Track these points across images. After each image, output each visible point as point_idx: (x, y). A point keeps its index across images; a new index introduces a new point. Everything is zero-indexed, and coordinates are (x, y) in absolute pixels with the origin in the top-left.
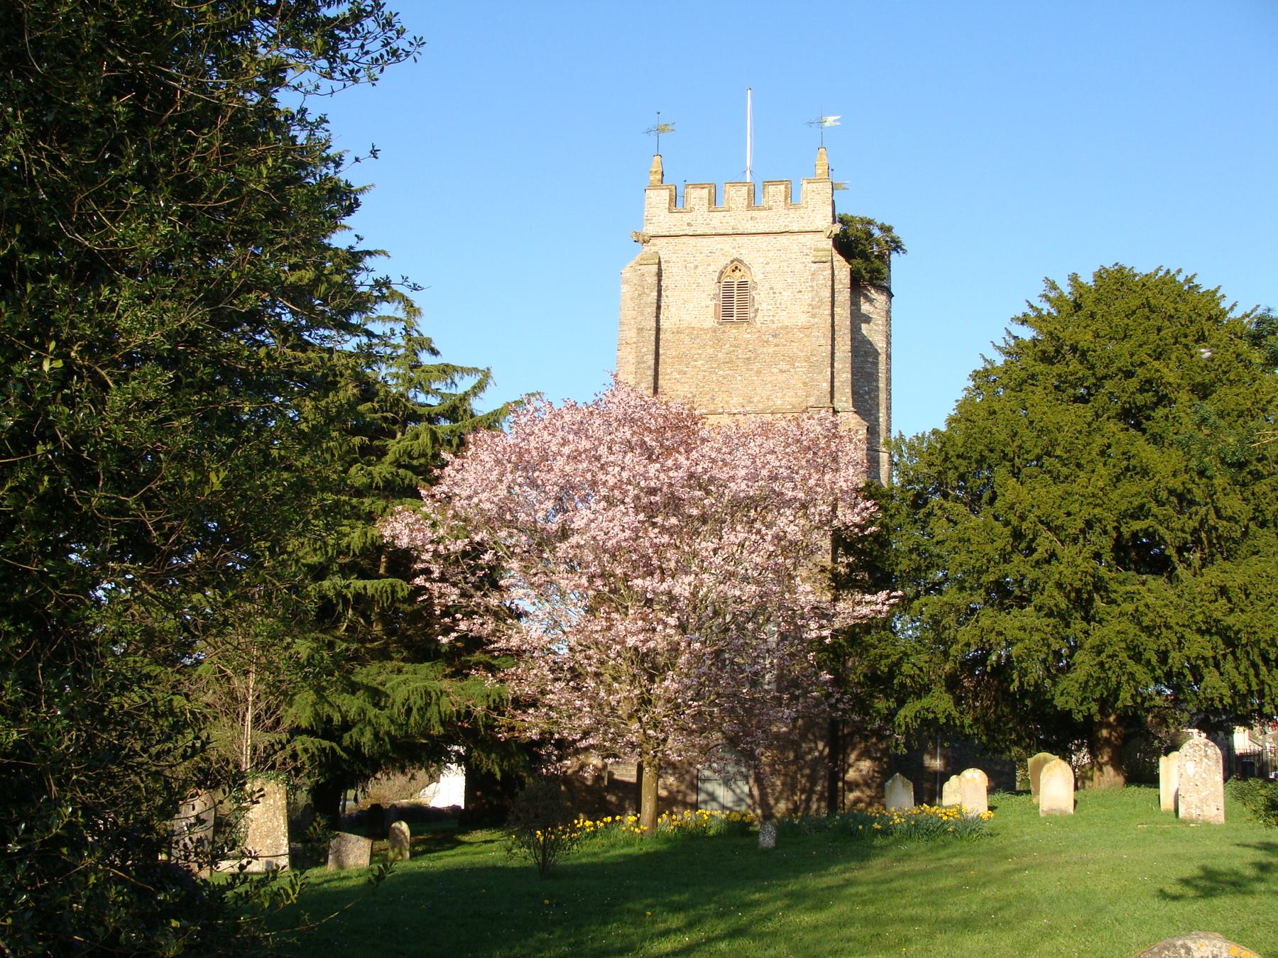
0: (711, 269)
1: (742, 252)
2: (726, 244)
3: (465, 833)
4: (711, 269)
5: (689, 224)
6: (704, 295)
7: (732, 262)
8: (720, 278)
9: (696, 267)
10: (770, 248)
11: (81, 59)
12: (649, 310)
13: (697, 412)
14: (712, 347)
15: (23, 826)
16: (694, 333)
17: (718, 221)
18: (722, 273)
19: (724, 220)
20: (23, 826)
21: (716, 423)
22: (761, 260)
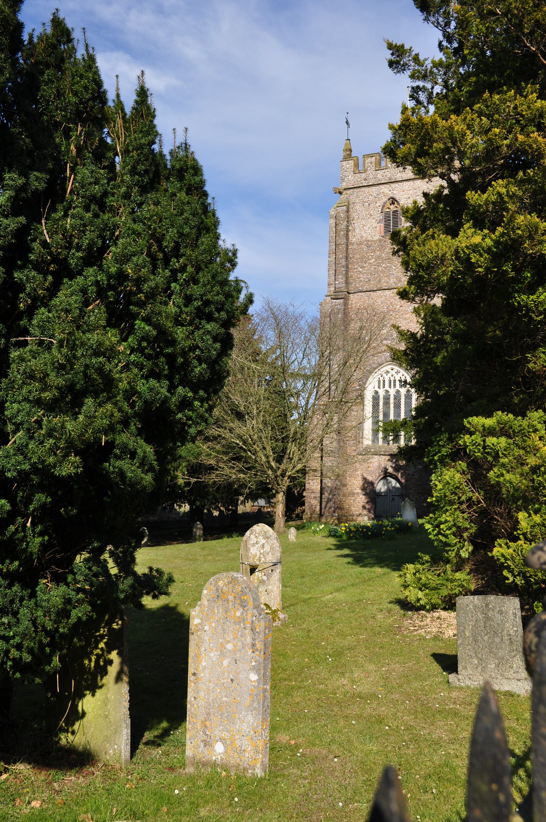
0: (378, 204)
1: (395, 192)
2: (385, 189)
3: (282, 573)
4: (378, 204)
5: (365, 179)
6: (374, 221)
7: (389, 199)
8: (382, 209)
9: (369, 204)
10: (410, 188)
11: (182, 188)
12: (342, 233)
13: (420, 93)
14: (378, 251)
15: (107, 617)
16: (369, 244)
17: (381, 176)
18: (383, 206)
19: (385, 175)
20: (107, 617)
21: (400, 260)
22: (405, 196)
